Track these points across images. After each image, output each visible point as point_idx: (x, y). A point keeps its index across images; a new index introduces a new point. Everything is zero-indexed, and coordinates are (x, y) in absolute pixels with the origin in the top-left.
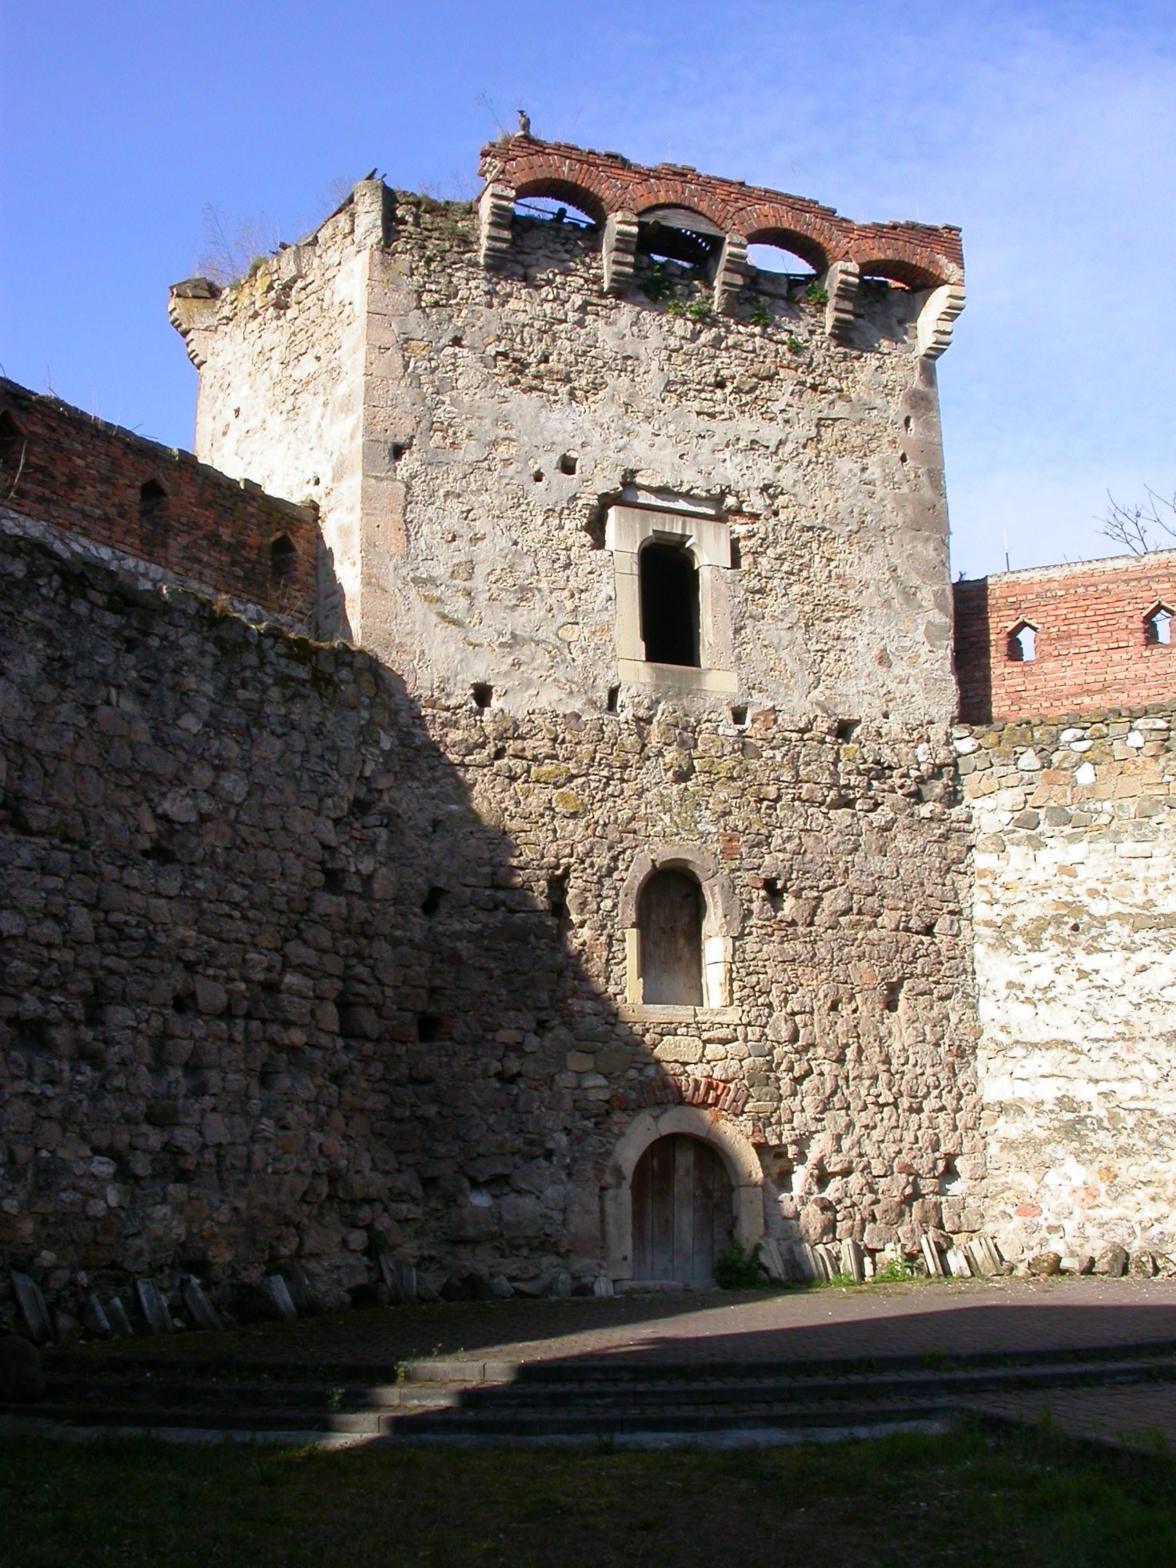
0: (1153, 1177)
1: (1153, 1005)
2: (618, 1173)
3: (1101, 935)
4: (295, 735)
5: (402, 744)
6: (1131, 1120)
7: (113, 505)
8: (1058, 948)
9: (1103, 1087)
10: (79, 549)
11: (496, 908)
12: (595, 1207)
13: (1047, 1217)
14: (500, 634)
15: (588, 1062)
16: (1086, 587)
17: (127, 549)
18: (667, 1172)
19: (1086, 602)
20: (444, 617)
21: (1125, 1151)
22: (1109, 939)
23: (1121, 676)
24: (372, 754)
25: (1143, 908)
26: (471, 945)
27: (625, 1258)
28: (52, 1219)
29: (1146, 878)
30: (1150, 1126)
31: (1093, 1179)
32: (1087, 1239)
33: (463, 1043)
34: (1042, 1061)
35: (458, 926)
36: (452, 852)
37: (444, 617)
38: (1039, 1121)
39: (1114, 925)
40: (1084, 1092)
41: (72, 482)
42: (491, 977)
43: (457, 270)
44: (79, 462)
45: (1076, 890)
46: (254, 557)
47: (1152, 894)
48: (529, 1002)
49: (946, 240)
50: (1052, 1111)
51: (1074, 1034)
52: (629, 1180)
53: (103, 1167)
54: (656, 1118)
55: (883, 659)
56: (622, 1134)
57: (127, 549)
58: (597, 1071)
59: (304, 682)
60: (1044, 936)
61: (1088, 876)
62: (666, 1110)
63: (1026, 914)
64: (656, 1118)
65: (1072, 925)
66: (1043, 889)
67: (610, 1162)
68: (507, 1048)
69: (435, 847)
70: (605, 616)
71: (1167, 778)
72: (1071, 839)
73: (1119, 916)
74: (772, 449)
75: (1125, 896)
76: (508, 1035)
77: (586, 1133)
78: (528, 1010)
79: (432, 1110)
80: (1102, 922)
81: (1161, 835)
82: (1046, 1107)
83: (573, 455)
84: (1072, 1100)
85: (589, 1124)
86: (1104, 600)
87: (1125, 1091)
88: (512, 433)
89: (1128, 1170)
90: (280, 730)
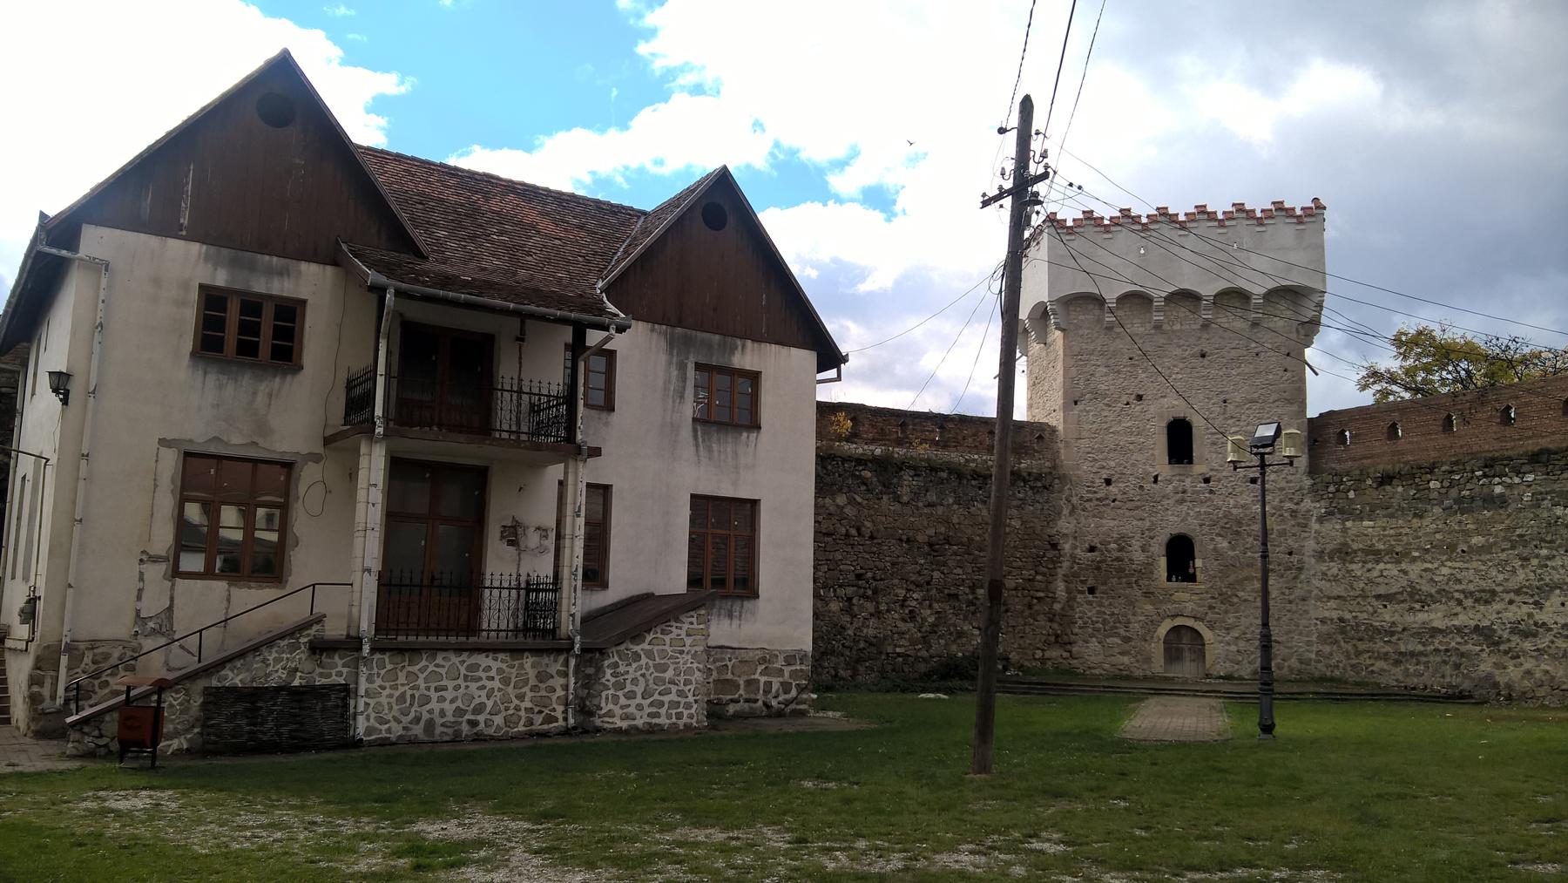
34: (1332, 604)
63: (1329, 547)
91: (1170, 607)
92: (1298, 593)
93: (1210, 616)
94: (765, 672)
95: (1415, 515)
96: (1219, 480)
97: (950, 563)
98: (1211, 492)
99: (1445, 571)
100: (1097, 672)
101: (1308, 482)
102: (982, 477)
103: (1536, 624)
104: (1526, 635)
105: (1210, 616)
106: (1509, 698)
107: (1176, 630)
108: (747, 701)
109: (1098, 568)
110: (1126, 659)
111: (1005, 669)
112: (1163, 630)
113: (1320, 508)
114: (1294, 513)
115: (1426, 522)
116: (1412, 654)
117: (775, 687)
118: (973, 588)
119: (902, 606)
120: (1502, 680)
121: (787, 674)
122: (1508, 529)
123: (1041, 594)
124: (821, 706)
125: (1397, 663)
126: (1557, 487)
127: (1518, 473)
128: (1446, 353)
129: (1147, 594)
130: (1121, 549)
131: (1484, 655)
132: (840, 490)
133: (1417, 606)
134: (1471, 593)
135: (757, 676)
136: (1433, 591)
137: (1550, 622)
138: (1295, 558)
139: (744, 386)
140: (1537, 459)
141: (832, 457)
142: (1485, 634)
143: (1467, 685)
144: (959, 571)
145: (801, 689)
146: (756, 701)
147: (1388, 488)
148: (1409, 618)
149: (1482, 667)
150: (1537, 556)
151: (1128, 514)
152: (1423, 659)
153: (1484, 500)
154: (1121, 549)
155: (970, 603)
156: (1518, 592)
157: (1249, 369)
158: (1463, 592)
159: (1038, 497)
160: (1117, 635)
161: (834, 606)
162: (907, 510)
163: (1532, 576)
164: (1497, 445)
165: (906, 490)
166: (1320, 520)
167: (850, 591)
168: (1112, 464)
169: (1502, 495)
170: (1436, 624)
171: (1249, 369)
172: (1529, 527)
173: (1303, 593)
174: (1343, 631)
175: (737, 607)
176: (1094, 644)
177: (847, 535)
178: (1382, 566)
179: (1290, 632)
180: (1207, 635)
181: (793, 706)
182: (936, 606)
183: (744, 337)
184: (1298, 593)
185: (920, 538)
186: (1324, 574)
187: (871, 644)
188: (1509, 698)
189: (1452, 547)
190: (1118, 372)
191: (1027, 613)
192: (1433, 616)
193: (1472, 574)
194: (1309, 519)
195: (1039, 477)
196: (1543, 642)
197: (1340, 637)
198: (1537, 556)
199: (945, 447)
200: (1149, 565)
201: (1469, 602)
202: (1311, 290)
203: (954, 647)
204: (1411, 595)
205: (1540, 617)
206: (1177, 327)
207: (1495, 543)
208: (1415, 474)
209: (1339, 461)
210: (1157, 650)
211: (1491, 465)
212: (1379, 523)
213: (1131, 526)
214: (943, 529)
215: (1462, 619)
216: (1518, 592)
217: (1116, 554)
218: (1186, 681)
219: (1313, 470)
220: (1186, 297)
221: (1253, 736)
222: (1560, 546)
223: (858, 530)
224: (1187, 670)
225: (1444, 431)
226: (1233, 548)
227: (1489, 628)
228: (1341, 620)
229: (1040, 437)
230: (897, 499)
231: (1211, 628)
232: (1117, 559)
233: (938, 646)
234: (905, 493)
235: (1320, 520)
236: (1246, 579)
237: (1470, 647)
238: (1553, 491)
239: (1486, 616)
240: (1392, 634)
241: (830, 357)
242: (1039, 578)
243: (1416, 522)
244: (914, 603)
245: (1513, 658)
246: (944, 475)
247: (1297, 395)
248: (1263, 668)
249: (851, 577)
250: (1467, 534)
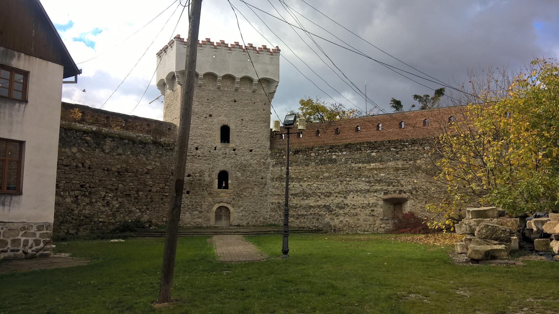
34: (276, 197)
41: (136, 126)
63: (276, 176)
91: (218, 199)
92: (264, 193)
93: (233, 202)
94: (25, 235)
95: (306, 165)
96: (239, 150)
97: (128, 181)
98: (236, 154)
99: (315, 185)
100: (188, 225)
101: (270, 152)
102: (144, 144)
103: (344, 204)
104: (341, 208)
105: (233, 202)
106: (335, 230)
107: (220, 208)
108: (12, 251)
109: (191, 184)
110: (200, 220)
111: (150, 226)
112: (215, 208)
113: (273, 162)
114: (264, 163)
115: (309, 168)
116: (303, 215)
117: (30, 243)
118: (137, 192)
119: (103, 200)
120: (332, 224)
121: (38, 236)
122: (337, 171)
123: (167, 194)
124: (58, 250)
125: (297, 218)
126: (353, 156)
127: (341, 151)
128: (317, 109)
129: (210, 194)
130: (200, 176)
131: (327, 215)
132: (74, 145)
133: (305, 198)
134: (324, 193)
135: (19, 237)
136: (311, 192)
137: (349, 203)
138: (264, 180)
139: (19, 77)
140: (347, 146)
141: (71, 129)
142: (327, 208)
143: (321, 226)
144: (131, 184)
145: (46, 243)
146: (18, 251)
147: (297, 155)
148: (302, 202)
149: (326, 220)
150: (346, 181)
151: (204, 162)
152: (306, 217)
153: (329, 161)
154: (200, 176)
155: (136, 198)
156: (339, 193)
157: (251, 108)
158: (321, 193)
159: (168, 153)
160: (197, 210)
161: (68, 200)
162: (108, 156)
163: (344, 187)
164: (333, 142)
165: (107, 147)
166: (273, 166)
167: (77, 193)
168: (199, 141)
169: (335, 159)
170: (311, 204)
171: (251, 108)
172: (343, 170)
173: (266, 193)
174: (279, 207)
175: (8, 199)
176: (188, 215)
177: (77, 167)
178: (294, 183)
179: (260, 208)
180: (231, 209)
181: (41, 252)
182: (120, 200)
183: (20, 51)
184: (264, 193)
185: (113, 169)
186: (274, 186)
187: (87, 218)
188: (335, 230)
189: (318, 177)
190: (203, 105)
191: (161, 202)
192: (310, 201)
193: (324, 187)
194: (269, 166)
195: (169, 145)
196: (346, 211)
197: (278, 209)
198: (346, 181)
199: (127, 129)
200: (211, 182)
201: (322, 197)
202: (275, 81)
203: (127, 218)
204: (303, 194)
205: (346, 202)
206: (226, 89)
207: (332, 176)
208: (307, 150)
209: (280, 145)
210: (212, 216)
211: (332, 148)
212: (294, 168)
213: (205, 167)
214: (125, 165)
215: (320, 203)
216: (339, 193)
217: (198, 178)
218: (223, 228)
219: (271, 148)
220: (229, 78)
221: (279, 256)
222: (353, 177)
223: (83, 164)
224: (223, 223)
225: (316, 136)
226: (242, 176)
227: (329, 206)
228: (279, 203)
229: (170, 129)
230: (103, 151)
231: (233, 207)
232: (199, 180)
233: (120, 217)
234: (107, 148)
235: (273, 166)
236: (246, 188)
237: (322, 212)
238: (352, 158)
239: (328, 201)
240: (296, 208)
241: (71, 70)
242: (166, 187)
243: (306, 168)
244: (109, 198)
245: (336, 216)
246: (126, 141)
247: (267, 120)
248: (285, 225)
249: (78, 186)
250: (323, 172)
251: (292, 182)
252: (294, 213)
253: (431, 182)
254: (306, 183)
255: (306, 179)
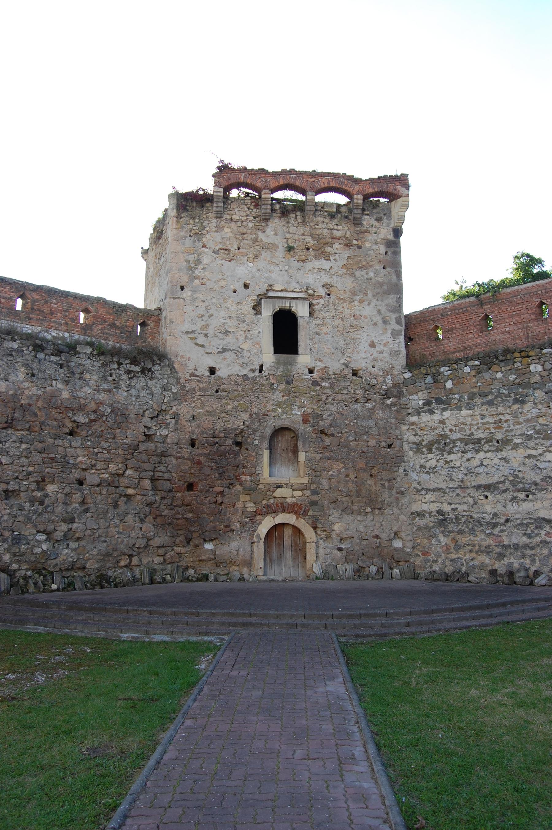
0: (470, 542)
1: (471, 474)
2: (258, 536)
3: (453, 447)
4: (133, 390)
5: (181, 389)
6: (463, 520)
7: (69, 318)
8: (438, 453)
9: (453, 506)
10: (55, 335)
11: (215, 444)
12: (249, 549)
13: (432, 557)
14: (218, 348)
15: (248, 498)
16: (459, 310)
17: (75, 332)
18: (281, 537)
19: (459, 316)
20: (197, 344)
21: (460, 532)
22: (456, 449)
23: (471, 344)
24: (168, 394)
25: (469, 436)
26: (205, 458)
27: (261, 568)
28: (18, 554)
29: (470, 424)
30: (470, 522)
31: (449, 542)
32: (446, 566)
33: (202, 492)
34: (430, 496)
35: (200, 452)
36: (199, 426)
37: (197, 344)
38: (430, 519)
39: (458, 443)
40: (447, 508)
41: (52, 313)
42: (212, 469)
43: (205, 220)
44: (54, 306)
45: (445, 429)
46: (130, 329)
47: (473, 430)
48: (226, 477)
49: (402, 180)
50: (435, 516)
51: (443, 486)
52: (263, 540)
53: (41, 537)
54: (274, 518)
55: (373, 345)
56: (260, 523)
57: (75, 332)
58: (250, 501)
59: (138, 372)
60: (434, 447)
61: (449, 424)
62: (277, 515)
63: (427, 439)
64: (274, 518)
65: (442, 444)
66: (433, 429)
67: (256, 534)
68: (218, 493)
69: (193, 424)
70: (258, 339)
71: (479, 384)
72: (444, 410)
73: (461, 440)
74: (328, 271)
75: (462, 431)
76: (219, 489)
77: (246, 523)
78: (226, 480)
79: (190, 515)
80: (454, 442)
81: (476, 407)
82: (433, 514)
83: (248, 282)
84: (442, 511)
85: (247, 520)
86: (465, 314)
87: (461, 508)
88: (225, 277)
89: (463, 539)
90: (126, 389)
95: (516, 401)
115: (528, 406)
116: (516, 547)
118: (41, 484)
133: (522, 495)
136: (538, 479)
148: (512, 508)
152: (529, 552)
178: (482, 455)
180: (309, 534)
192: (538, 505)
251: (477, 452)
252: (490, 541)
253: (465, 708)
254: (521, 453)
255: (519, 441)
